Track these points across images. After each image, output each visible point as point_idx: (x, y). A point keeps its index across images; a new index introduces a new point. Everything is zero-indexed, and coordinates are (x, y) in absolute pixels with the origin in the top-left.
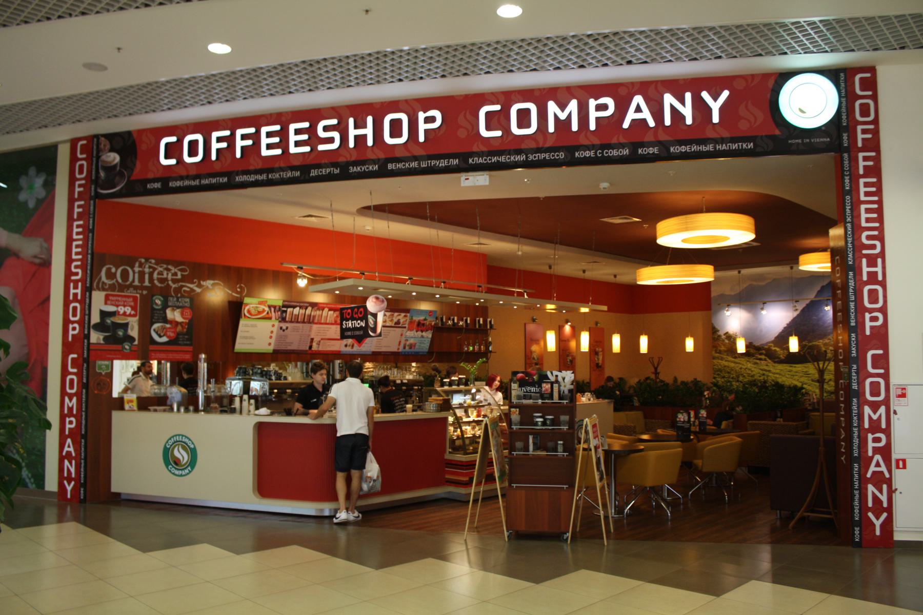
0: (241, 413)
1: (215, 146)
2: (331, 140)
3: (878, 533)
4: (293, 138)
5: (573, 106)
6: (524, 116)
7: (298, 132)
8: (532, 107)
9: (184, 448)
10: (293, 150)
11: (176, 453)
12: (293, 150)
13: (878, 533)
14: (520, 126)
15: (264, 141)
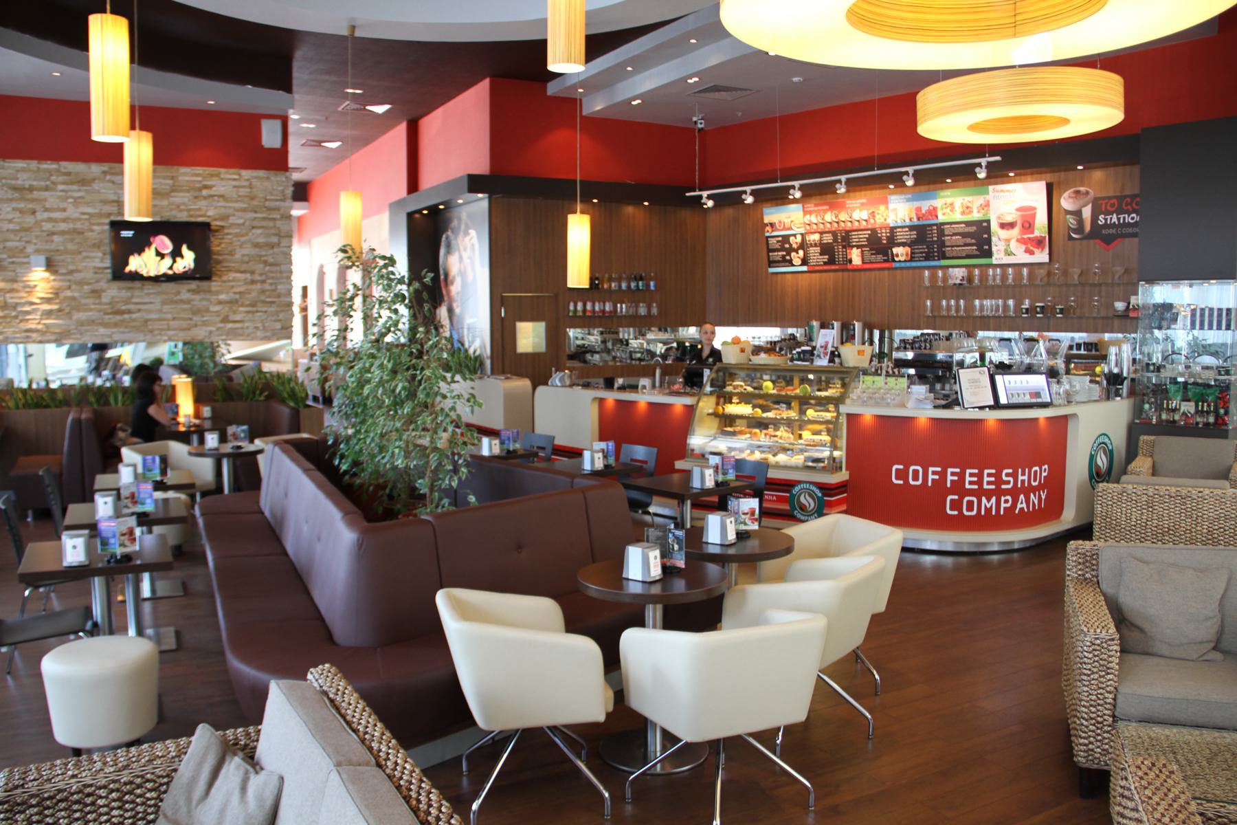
0: (1193, 312)
1: (931, 477)
2: (1008, 482)
3: (998, 158)
4: (986, 479)
5: (994, 499)
6: (970, 504)
7: (989, 475)
8: (975, 499)
9: (810, 495)
10: (985, 486)
11: (802, 499)
12: (985, 486)
13: (998, 158)
14: (968, 510)
15: (968, 479)
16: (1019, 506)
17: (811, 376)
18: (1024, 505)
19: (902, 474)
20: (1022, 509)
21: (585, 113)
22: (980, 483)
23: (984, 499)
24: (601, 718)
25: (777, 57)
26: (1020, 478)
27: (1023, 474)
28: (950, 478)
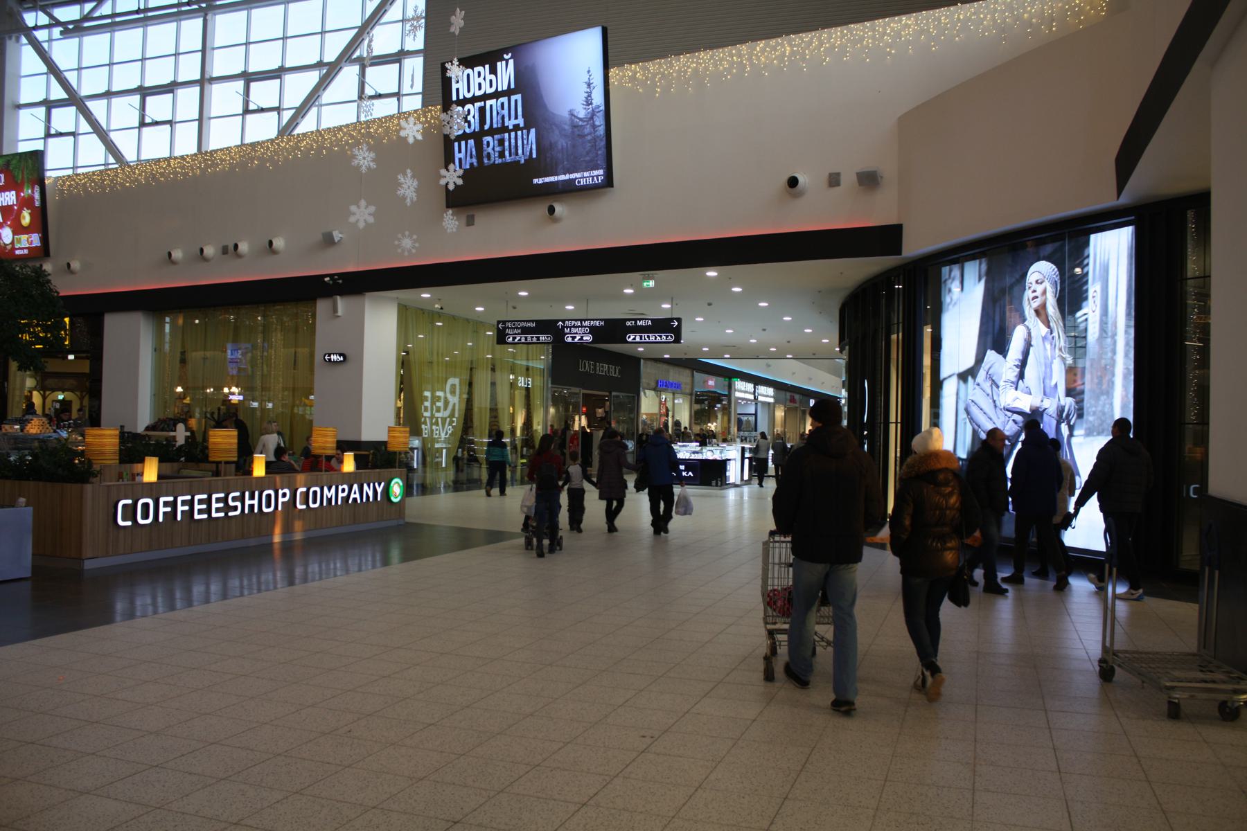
2: (235, 508)
10: (214, 515)
16: (353, 496)
17: (71, 27)
18: (357, 496)
19: (130, 512)
20: (355, 499)
21: (1196, 606)
22: (209, 511)
23: (326, 489)
24: (1092, 237)
25: (1098, 458)
26: (248, 502)
27: (252, 497)
28: (180, 508)
